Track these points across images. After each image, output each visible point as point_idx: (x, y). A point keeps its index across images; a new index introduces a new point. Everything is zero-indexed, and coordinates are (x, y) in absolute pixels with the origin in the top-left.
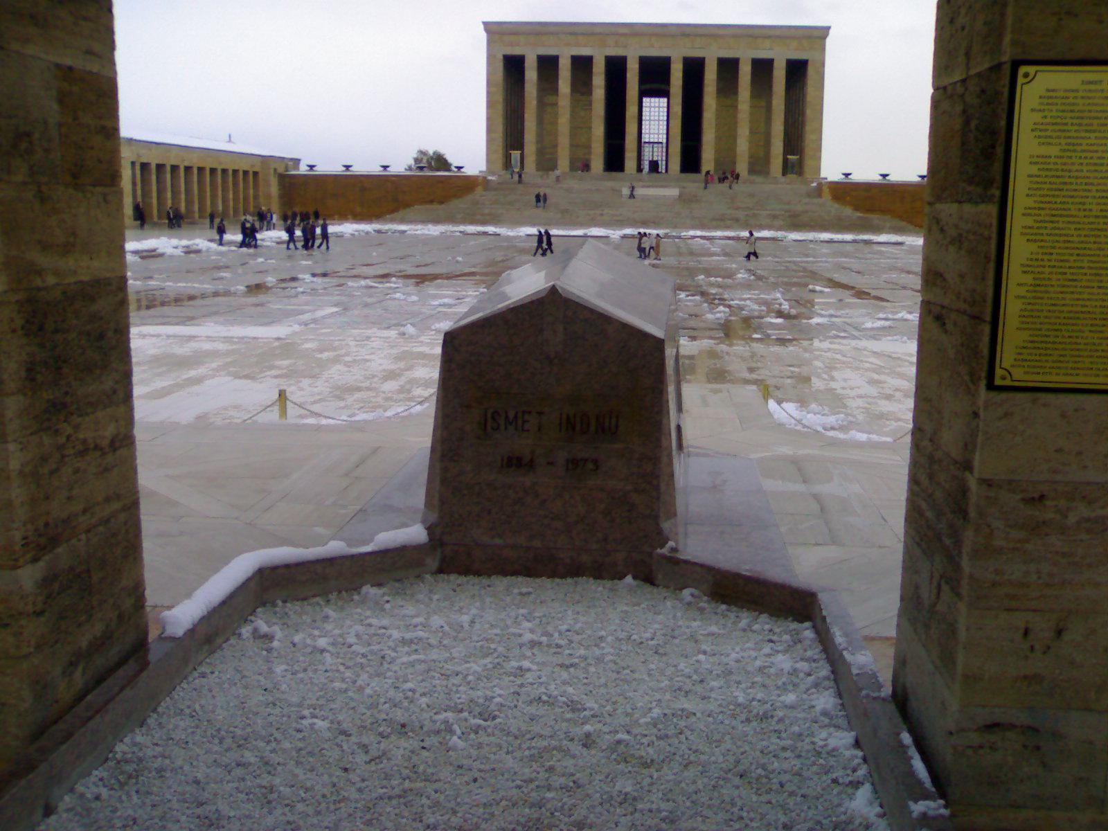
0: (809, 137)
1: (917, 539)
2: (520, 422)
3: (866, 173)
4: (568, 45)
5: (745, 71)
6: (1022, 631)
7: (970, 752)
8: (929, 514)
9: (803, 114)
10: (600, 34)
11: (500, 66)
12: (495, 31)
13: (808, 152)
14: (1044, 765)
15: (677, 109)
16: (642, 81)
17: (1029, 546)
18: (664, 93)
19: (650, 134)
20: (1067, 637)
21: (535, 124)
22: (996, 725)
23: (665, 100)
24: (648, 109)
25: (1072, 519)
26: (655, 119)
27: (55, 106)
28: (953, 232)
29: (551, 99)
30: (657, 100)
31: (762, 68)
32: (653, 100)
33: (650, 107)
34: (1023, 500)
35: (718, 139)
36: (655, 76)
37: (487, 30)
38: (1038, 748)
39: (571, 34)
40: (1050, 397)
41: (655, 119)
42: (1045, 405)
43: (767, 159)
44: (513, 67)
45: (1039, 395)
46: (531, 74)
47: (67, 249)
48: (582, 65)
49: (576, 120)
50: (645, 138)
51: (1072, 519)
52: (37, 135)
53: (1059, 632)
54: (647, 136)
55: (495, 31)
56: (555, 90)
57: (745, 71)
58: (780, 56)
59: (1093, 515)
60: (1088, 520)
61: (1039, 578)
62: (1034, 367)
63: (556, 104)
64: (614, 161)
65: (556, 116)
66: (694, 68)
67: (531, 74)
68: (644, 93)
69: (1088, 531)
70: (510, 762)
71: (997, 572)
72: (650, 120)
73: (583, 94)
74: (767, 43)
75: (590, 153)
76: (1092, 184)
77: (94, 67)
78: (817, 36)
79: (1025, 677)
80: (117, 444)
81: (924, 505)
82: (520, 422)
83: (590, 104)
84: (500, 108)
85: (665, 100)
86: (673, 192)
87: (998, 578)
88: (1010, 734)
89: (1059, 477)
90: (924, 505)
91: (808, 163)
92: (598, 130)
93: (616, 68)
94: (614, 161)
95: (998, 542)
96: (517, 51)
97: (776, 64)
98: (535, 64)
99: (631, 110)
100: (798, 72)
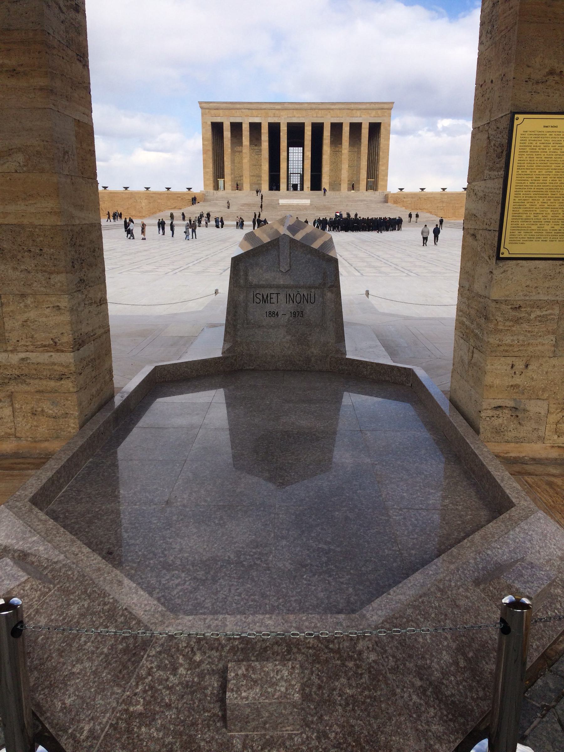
0: (381, 168)
1: (461, 335)
2: (269, 298)
3: (411, 188)
4: (247, 116)
5: (346, 130)
6: (511, 366)
7: (488, 419)
8: (467, 323)
9: (378, 155)
10: (265, 109)
11: (209, 128)
12: (206, 107)
13: (381, 177)
14: (520, 423)
15: (308, 154)
16: (288, 139)
17: (514, 329)
18: (301, 144)
19: (293, 168)
20: (530, 367)
21: (230, 163)
22: (500, 407)
23: (302, 148)
24: (292, 154)
25: (533, 316)
26: (296, 159)
27: (75, 139)
28: (481, 194)
29: (239, 149)
30: (297, 148)
31: (356, 128)
32: (295, 148)
33: (293, 153)
34: (511, 308)
35: (331, 170)
36: (296, 134)
37: (202, 108)
38: (517, 416)
39: (249, 109)
40: (524, 262)
41: (296, 159)
42: (521, 267)
43: (358, 181)
44: (217, 128)
45: (519, 262)
46: (227, 134)
47: (81, 208)
48: (255, 128)
49: (250, 161)
50: (291, 171)
51: (533, 316)
52: (70, 153)
53: (527, 366)
54: (292, 170)
55: (206, 107)
56: (241, 143)
57: (346, 130)
58: (365, 121)
59: (542, 314)
60: (540, 316)
61: (518, 342)
62: (521, 178)
63: (241, 152)
64: (274, 184)
65: (242, 158)
66: (318, 129)
67: (227, 134)
68: (290, 144)
69: (540, 321)
70: (508, 339)
71: (500, 340)
72: (293, 161)
73: (256, 145)
74: (358, 113)
75: (261, 180)
76: (542, 183)
77: (86, 121)
78: (386, 108)
79: (512, 386)
80: (102, 302)
81: (465, 320)
82: (269, 298)
83: (260, 150)
84: (210, 154)
85: (302, 148)
86: (307, 202)
87: (500, 343)
88: (506, 411)
89: (527, 298)
90: (465, 320)
91: (380, 183)
92: (265, 167)
93: (274, 129)
94: (274, 184)
95: (500, 327)
96: (218, 120)
97: (363, 126)
98: (229, 128)
99: (283, 155)
100: (375, 129)
